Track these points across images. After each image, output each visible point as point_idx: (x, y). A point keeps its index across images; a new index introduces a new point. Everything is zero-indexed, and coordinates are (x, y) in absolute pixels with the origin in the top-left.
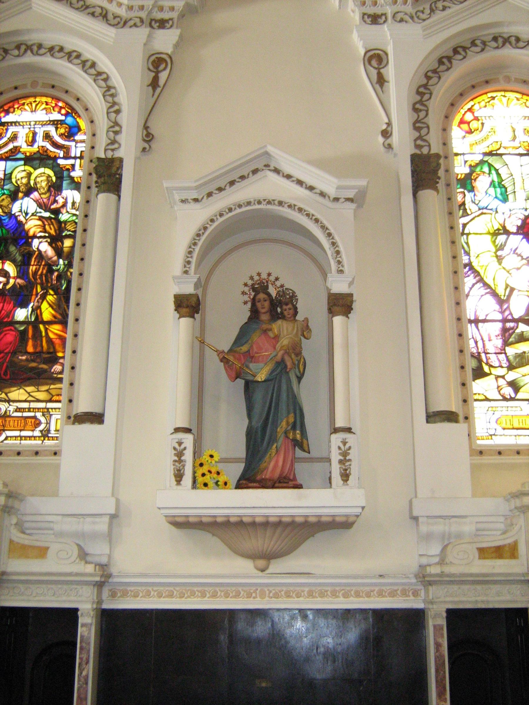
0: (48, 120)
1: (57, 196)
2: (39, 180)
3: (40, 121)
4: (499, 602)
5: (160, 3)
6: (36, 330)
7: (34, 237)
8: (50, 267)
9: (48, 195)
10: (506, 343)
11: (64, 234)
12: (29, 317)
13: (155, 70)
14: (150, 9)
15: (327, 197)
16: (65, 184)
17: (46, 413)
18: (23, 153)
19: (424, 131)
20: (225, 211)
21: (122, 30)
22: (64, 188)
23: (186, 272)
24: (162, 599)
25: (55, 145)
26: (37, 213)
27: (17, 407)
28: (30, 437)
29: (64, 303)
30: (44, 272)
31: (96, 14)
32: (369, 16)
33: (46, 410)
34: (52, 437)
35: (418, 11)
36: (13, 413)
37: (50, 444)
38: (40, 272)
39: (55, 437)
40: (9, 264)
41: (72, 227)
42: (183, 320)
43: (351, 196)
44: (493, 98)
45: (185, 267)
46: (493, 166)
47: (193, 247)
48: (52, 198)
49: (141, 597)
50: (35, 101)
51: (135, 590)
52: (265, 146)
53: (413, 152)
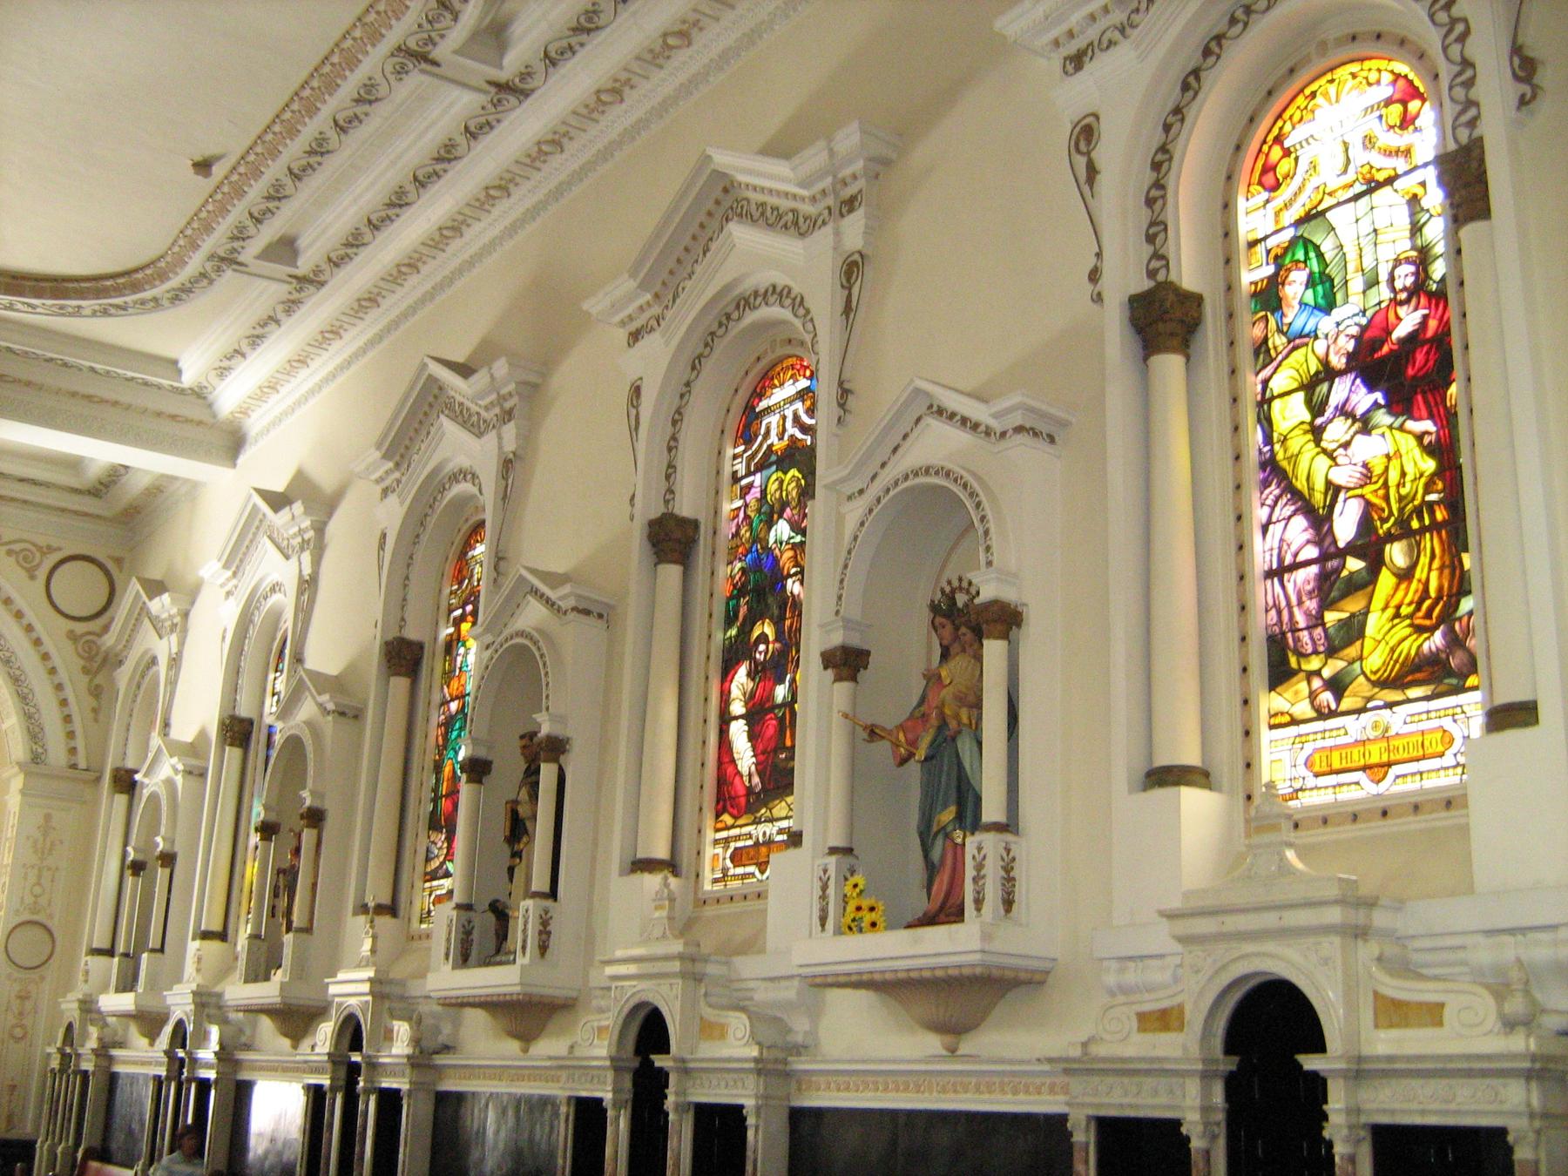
2: (790, 488)
4: (1153, 1107)
10: (1326, 604)
42: (838, 685)
44: (1313, 95)
46: (1311, 242)
52: (912, 380)
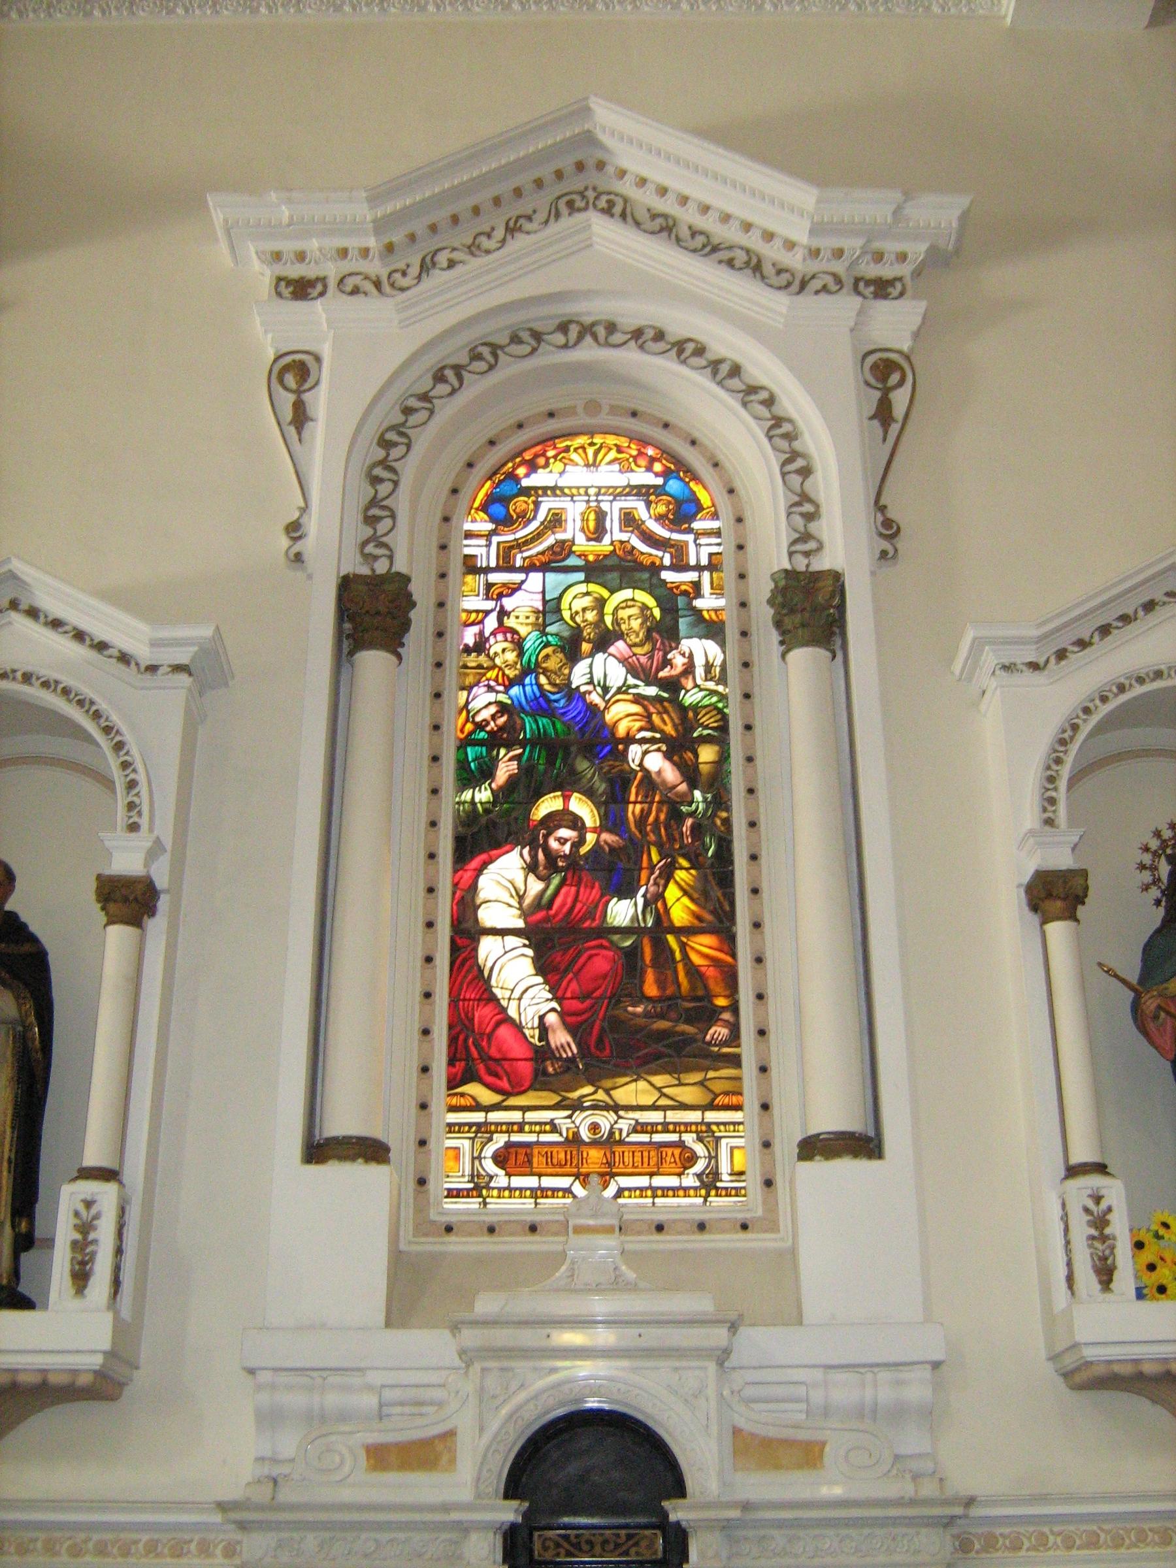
0: (626, 484)
1: (670, 652)
2: (623, 614)
3: (609, 488)
5: (877, 245)
6: (660, 946)
7: (629, 740)
8: (674, 809)
9: (647, 647)
11: (695, 735)
12: (640, 917)
13: (879, 386)
14: (855, 256)
15: (133, 664)
16: (683, 624)
17: (705, 1135)
18: (579, 556)
19: (383, 527)
20: (1110, 691)
21: (795, 298)
22: (682, 634)
23: (1049, 822)
24: (1074, 1552)
25: (649, 538)
26: (629, 687)
27: (637, 1121)
28: (673, 1189)
29: (716, 888)
30: (662, 817)
31: (738, 264)
32: (289, 282)
33: (704, 1128)
34: (726, 1189)
35: (395, 271)
36: (628, 1136)
37: (721, 1204)
38: (651, 819)
39: (732, 1188)
40: (580, 799)
41: (712, 720)
43: (184, 660)
45: (1045, 810)
47: (1055, 767)
48: (658, 655)
49: (1028, 1550)
50: (592, 444)
51: (1010, 1533)
53: (347, 569)
